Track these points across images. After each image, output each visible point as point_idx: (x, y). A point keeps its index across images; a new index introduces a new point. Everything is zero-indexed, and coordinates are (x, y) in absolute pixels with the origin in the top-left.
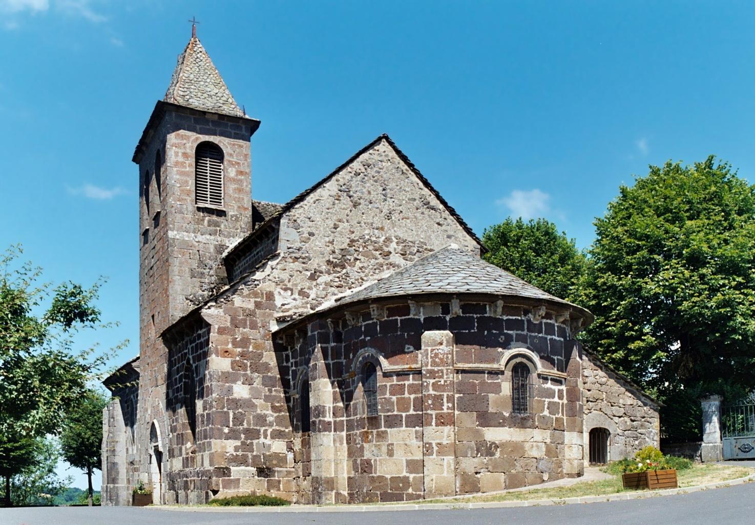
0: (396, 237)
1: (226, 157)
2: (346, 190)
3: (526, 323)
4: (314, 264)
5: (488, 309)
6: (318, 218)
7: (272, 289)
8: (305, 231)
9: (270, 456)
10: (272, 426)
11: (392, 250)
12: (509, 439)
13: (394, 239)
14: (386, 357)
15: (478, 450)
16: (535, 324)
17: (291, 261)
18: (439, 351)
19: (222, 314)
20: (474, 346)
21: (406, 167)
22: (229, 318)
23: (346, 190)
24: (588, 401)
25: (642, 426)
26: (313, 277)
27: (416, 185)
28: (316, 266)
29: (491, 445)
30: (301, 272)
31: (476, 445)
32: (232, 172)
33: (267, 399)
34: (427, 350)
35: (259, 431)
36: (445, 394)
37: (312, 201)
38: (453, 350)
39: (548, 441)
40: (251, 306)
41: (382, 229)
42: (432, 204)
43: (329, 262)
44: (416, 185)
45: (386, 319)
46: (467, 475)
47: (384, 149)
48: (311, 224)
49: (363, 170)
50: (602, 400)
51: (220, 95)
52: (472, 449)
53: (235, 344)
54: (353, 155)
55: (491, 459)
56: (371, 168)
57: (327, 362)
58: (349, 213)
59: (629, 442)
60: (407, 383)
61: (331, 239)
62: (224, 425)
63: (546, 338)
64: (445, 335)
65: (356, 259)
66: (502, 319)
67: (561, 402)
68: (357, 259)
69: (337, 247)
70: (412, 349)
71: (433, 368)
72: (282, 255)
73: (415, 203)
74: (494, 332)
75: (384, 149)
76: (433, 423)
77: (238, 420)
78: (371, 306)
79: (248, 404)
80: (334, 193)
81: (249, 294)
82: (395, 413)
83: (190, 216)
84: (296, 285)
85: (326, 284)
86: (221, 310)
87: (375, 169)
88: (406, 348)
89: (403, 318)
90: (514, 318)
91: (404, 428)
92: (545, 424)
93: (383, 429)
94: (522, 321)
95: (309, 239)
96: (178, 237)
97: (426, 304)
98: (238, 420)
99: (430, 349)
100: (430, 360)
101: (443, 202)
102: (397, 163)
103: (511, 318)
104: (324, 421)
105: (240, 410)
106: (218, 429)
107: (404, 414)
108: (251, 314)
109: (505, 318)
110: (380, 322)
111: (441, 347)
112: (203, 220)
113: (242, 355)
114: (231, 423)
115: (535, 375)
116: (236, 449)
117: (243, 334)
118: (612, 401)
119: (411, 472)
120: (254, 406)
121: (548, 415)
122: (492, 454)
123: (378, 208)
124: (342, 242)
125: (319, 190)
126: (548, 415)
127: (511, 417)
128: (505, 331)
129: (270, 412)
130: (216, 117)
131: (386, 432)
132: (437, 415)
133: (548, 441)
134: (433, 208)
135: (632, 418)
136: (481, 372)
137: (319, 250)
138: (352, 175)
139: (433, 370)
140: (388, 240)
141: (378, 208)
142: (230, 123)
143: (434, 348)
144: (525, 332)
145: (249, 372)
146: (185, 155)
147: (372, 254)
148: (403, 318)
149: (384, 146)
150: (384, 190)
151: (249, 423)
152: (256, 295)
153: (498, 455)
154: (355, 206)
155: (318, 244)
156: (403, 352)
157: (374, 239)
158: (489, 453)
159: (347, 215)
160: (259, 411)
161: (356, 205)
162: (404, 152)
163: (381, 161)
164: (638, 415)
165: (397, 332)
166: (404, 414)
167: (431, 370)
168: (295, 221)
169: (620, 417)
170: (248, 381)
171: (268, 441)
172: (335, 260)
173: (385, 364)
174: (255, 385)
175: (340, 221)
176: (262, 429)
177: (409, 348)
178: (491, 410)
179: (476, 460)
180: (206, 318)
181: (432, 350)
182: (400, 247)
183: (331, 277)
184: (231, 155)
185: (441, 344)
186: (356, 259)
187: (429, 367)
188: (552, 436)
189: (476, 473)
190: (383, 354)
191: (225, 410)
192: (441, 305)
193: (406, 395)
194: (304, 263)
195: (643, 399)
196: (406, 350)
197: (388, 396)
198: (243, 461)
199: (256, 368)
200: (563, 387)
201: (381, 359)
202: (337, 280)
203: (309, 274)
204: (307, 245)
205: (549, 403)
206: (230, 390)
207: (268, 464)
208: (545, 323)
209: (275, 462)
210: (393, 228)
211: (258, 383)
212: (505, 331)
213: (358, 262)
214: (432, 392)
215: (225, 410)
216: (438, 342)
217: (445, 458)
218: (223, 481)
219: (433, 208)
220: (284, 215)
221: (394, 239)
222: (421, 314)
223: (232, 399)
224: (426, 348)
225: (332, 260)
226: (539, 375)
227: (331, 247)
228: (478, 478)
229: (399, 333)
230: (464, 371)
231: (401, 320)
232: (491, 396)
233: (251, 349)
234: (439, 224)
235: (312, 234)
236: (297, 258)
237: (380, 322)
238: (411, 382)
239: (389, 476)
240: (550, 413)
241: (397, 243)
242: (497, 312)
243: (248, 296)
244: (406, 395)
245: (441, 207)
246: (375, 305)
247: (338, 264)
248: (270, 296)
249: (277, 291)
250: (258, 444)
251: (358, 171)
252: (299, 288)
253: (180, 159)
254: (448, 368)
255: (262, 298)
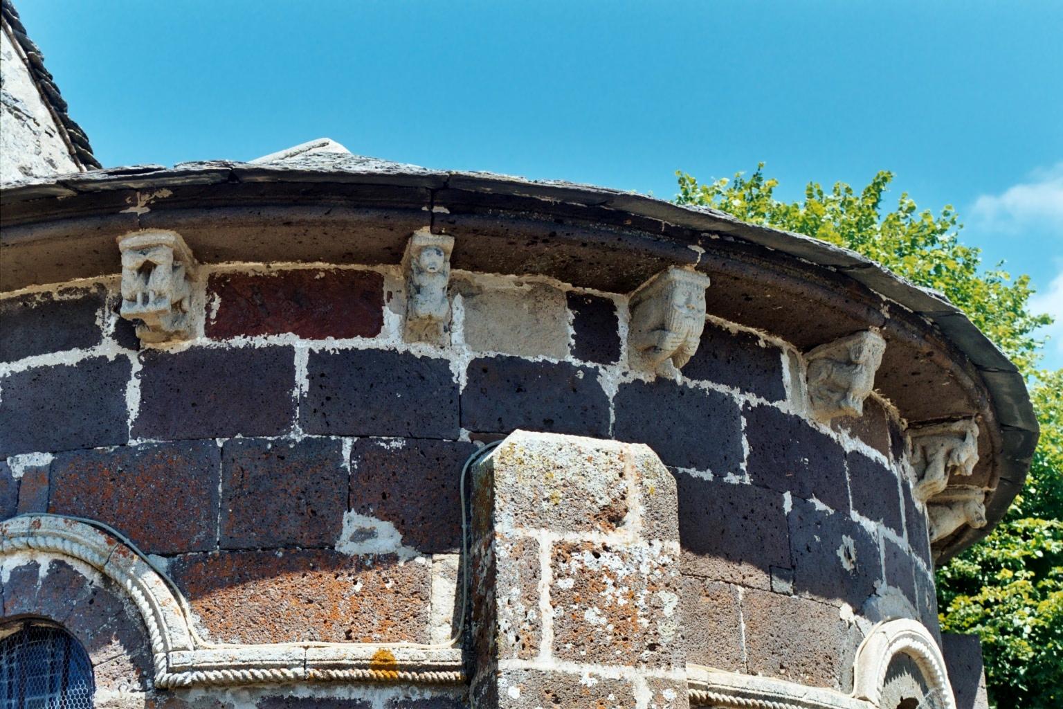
14: (189, 582)
18: (605, 558)
20: (745, 568)
34: (531, 546)
45: (202, 341)
70: (387, 537)
71: (571, 668)
78: (128, 241)
88: (348, 531)
89: (332, 344)
99: (547, 539)
100: (548, 614)
101: (51, 98)
110: (154, 361)
111: (614, 538)
139: (572, 683)
143: (571, 538)
148: (332, 344)
156: (321, 554)
165: (285, 425)
167: (556, 677)
177: (363, 535)
181: (563, 552)
185: (615, 519)
187: (546, 661)
190: (163, 563)
192: (574, 301)
196: (346, 546)
201: (150, 589)
216: (579, 500)
222: (457, 335)
224: (520, 533)
229: (297, 435)
231: (316, 359)
237: (154, 361)
245: (42, 113)
246: (168, 237)
254: (660, 673)
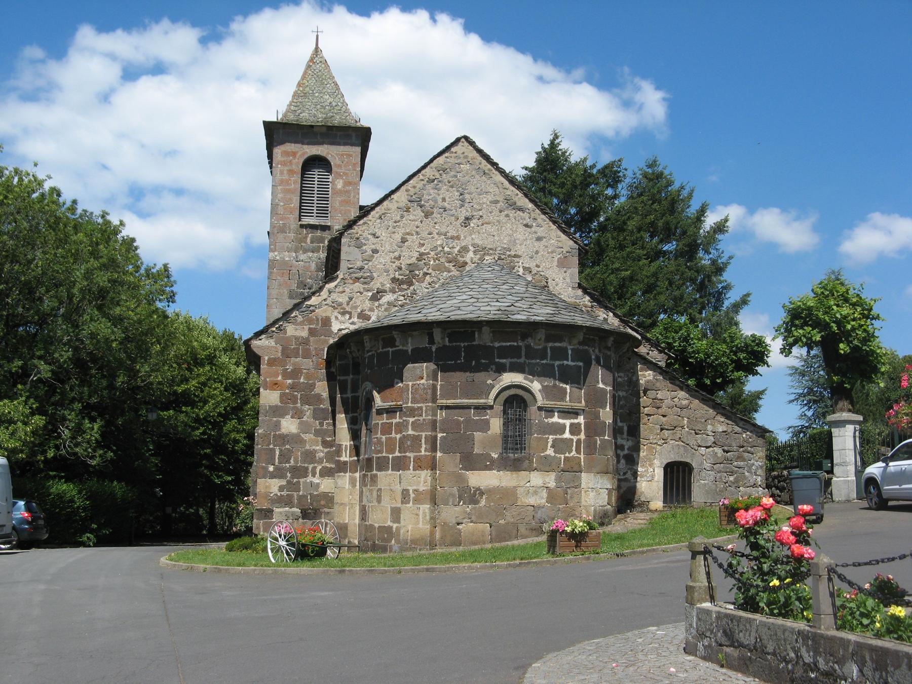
0: (473, 245)
1: (334, 169)
2: (417, 201)
3: (523, 349)
4: (376, 285)
5: (476, 336)
6: (383, 234)
7: (328, 314)
8: (368, 248)
9: (318, 495)
10: (322, 463)
11: (468, 261)
12: (498, 484)
13: (471, 248)
15: (460, 498)
16: (537, 350)
17: (351, 282)
19: (273, 344)
21: (489, 166)
22: (280, 348)
23: (417, 201)
24: (662, 429)
25: (738, 457)
26: (375, 298)
27: (500, 186)
28: (379, 285)
29: (475, 491)
30: (361, 293)
31: (458, 491)
32: (340, 184)
33: (317, 433)
35: (307, 468)
36: (424, 434)
37: (377, 216)
38: (434, 388)
39: (552, 484)
40: (304, 333)
41: (458, 238)
42: (519, 204)
43: (394, 280)
44: (500, 186)
46: (448, 526)
47: (464, 149)
48: (375, 240)
49: (438, 176)
50: (683, 427)
51: (334, 104)
52: (454, 496)
53: (286, 375)
54: (427, 160)
55: (474, 508)
56: (448, 173)
57: (345, 396)
58: (419, 224)
59: (721, 478)
60: (394, 421)
61: (397, 254)
62: (269, 463)
63: (553, 365)
64: (425, 368)
65: (426, 274)
66: (493, 347)
67: (575, 438)
68: (428, 274)
69: (404, 262)
72: (341, 276)
73: (498, 205)
74: (483, 361)
75: (464, 149)
76: (411, 468)
77: (285, 457)
79: (295, 439)
80: (402, 205)
81: (303, 321)
82: (384, 454)
83: (292, 235)
84: (356, 307)
85: (389, 303)
86: (271, 341)
87: (452, 173)
90: (509, 344)
91: (390, 472)
92: (547, 465)
93: (375, 472)
94: (519, 347)
95: (373, 257)
96: (278, 258)
97: (414, 333)
98: (285, 457)
102: (477, 163)
103: (504, 344)
104: (339, 461)
105: (287, 447)
106: (263, 468)
107: (391, 456)
108: (305, 342)
109: (497, 345)
112: (306, 237)
113: (292, 387)
114: (277, 461)
115: (533, 409)
116: (281, 488)
117: (294, 364)
118: (697, 428)
119: (394, 522)
120: (303, 442)
121: (553, 454)
122: (476, 502)
123: (452, 215)
124: (409, 257)
125: (385, 203)
126: (553, 454)
127: (501, 457)
128: (497, 360)
129: (320, 447)
130: (324, 129)
131: (376, 476)
132: (415, 457)
133: (552, 484)
134: (521, 209)
135: (726, 448)
136: (468, 407)
137: (383, 270)
138: (425, 182)
140: (465, 249)
141: (452, 215)
142: (339, 133)
144: (522, 360)
145: (299, 405)
146: (291, 172)
147: (445, 267)
149: (462, 147)
150: (461, 194)
151: (296, 461)
152: (310, 321)
153: (483, 503)
154: (426, 216)
155: (382, 260)
157: (446, 249)
158: (473, 500)
159: (417, 227)
160: (308, 447)
161: (427, 215)
162: (487, 151)
163: (459, 164)
164: (734, 444)
166: (391, 456)
168: (358, 239)
169: (707, 447)
170: (298, 414)
171: (316, 480)
172: (401, 277)
173: (378, 401)
174: (305, 418)
175: (408, 234)
176: (311, 466)
178: (476, 451)
179: (457, 509)
180: (255, 350)
182: (478, 256)
183: (395, 296)
184: (339, 166)
186: (426, 274)
188: (558, 480)
189: (458, 524)
191: (271, 446)
193: (393, 435)
194: (365, 283)
195: (741, 423)
197: (379, 435)
198: (286, 501)
199: (307, 400)
200: (581, 420)
201: (375, 393)
202: (402, 298)
203: (370, 294)
204: (370, 263)
205: (554, 441)
206: (277, 425)
207: (315, 504)
208: (551, 348)
209: (323, 503)
210: (471, 235)
211: (308, 416)
212: (497, 360)
213: (428, 277)
214: (411, 432)
215: (271, 446)
217: (421, 506)
218: (264, 524)
219: (521, 209)
220: (346, 234)
221: (471, 248)
223: (280, 435)
225: (397, 276)
226: (540, 409)
227: (397, 263)
228: (460, 530)
230: (448, 407)
232: (478, 435)
233: (302, 380)
234: (526, 226)
235: (375, 251)
236: (358, 279)
238: (398, 420)
239: (377, 525)
240: (555, 452)
241: (474, 252)
242: (484, 338)
243: (302, 323)
244: (393, 435)
247: (405, 280)
248: (327, 322)
249: (334, 315)
250: (305, 482)
251: (432, 177)
252: (359, 310)
253: (286, 177)
255: (317, 324)
